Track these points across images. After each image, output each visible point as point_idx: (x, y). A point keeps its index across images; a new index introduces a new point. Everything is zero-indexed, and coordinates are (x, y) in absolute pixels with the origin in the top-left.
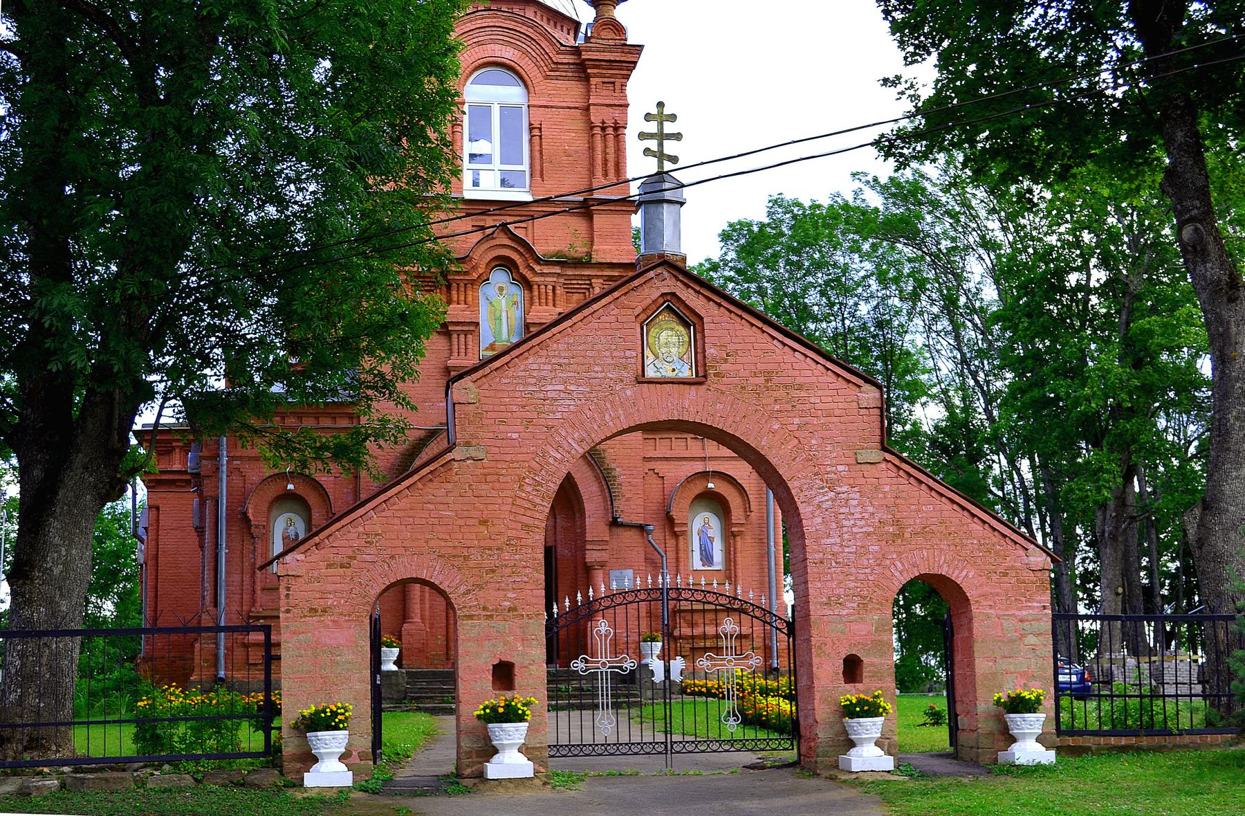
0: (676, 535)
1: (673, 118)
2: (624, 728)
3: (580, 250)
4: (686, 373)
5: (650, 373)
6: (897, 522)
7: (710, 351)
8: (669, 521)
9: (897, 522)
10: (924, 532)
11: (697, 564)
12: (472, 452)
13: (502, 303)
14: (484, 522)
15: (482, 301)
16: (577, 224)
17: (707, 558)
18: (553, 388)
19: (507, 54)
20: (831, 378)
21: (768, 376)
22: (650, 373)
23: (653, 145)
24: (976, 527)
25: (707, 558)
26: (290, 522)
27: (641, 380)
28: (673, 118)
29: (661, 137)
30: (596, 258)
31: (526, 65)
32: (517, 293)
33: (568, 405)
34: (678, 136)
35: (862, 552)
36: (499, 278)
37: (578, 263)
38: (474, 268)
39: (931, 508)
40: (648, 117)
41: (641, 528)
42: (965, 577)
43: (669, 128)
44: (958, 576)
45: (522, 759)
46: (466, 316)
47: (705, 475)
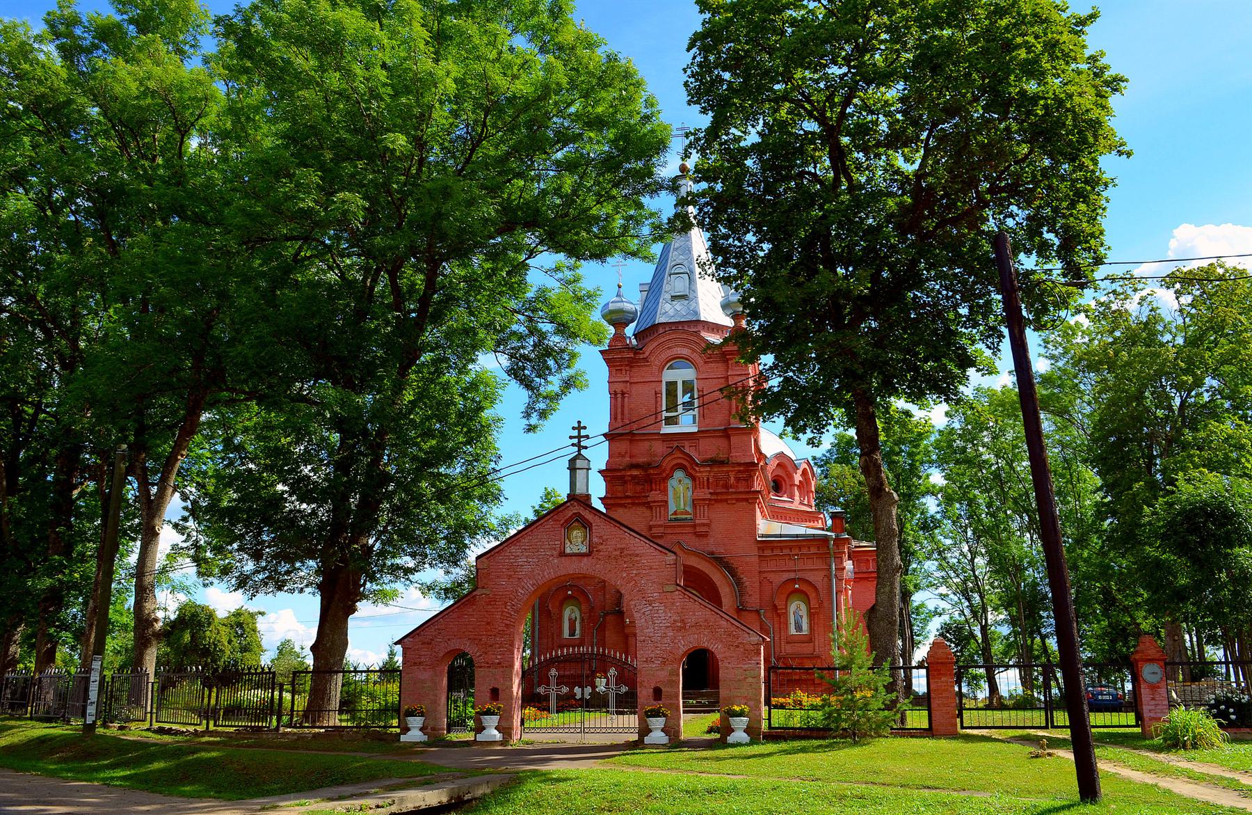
0: (779, 615)
1: (585, 428)
2: (604, 720)
3: (722, 456)
4: (584, 550)
5: (568, 551)
6: (682, 621)
7: (595, 540)
8: (775, 608)
9: (682, 621)
10: (697, 625)
11: (793, 631)
12: (484, 591)
13: (681, 488)
14: (488, 623)
15: (670, 489)
16: (722, 443)
17: (799, 628)
18: (521, 560)
19: (685, 352)
20: (652, 550)
21: (622, 550)
22: (568, 551)
23: (575, 441)
24: (723, 623)
25: (799, 628)
26: (573, 611)
27: (562, 554)
28: (585, 428)
29: (579, 437)
30: (734, 460)
31: (695, 356)
32: (688, 482)
33: (527, 568)
34: (571, 437)
35: (664, 636)
36: (679, 474)
37: (722, 463)
38: (664, 471)
39: (699, 611)
40: (574, 428)
41: (757, 612)
42: (717, 648)
43: (583, 433)
44: (712, 648)
45: (496, 732)
46: (660, 497)
47: (794, 581)
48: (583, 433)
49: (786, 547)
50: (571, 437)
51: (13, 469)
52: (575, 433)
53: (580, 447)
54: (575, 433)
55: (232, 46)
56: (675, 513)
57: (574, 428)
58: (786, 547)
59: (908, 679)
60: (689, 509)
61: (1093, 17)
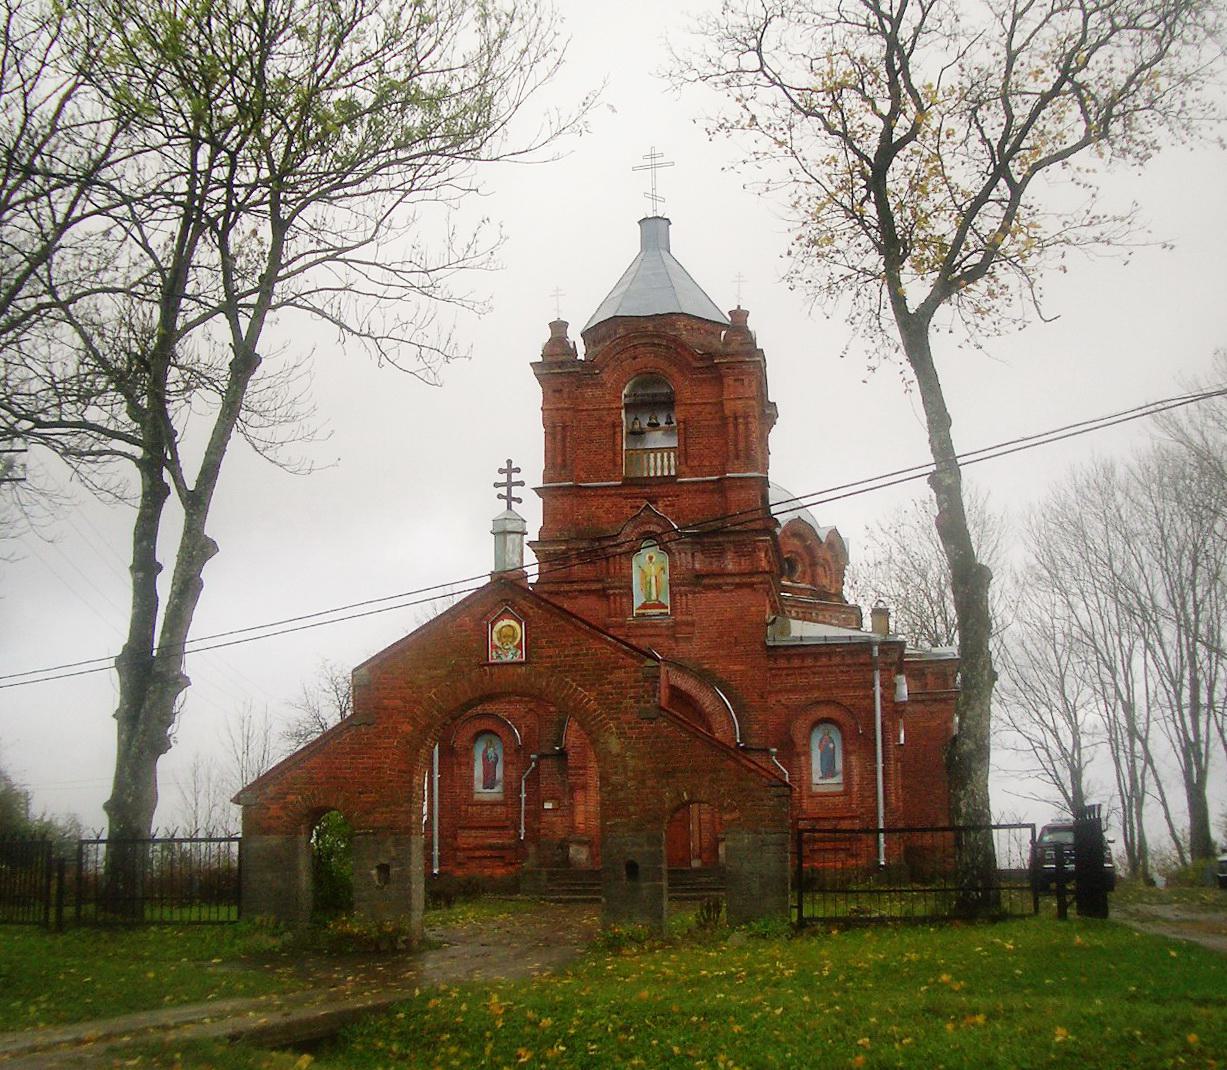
1: (518, 470)
13: (653, 570)
23: (503, 491)
28: (518, 470)
34: (497, 485)
40: (501, 471)
43: (515, 477)
48: (515, 477)
49: (809, 654)
50: (497, 485)
51: (679, 1061)
52: (503, 478)
53: (510, 499)
54: (503, 478)
55: (972, 702)
56: (644, 606)
57: (501, 471)
58: (809, 654)
59: (294, 794)
60: (666, 600)
61: (655, 230)
